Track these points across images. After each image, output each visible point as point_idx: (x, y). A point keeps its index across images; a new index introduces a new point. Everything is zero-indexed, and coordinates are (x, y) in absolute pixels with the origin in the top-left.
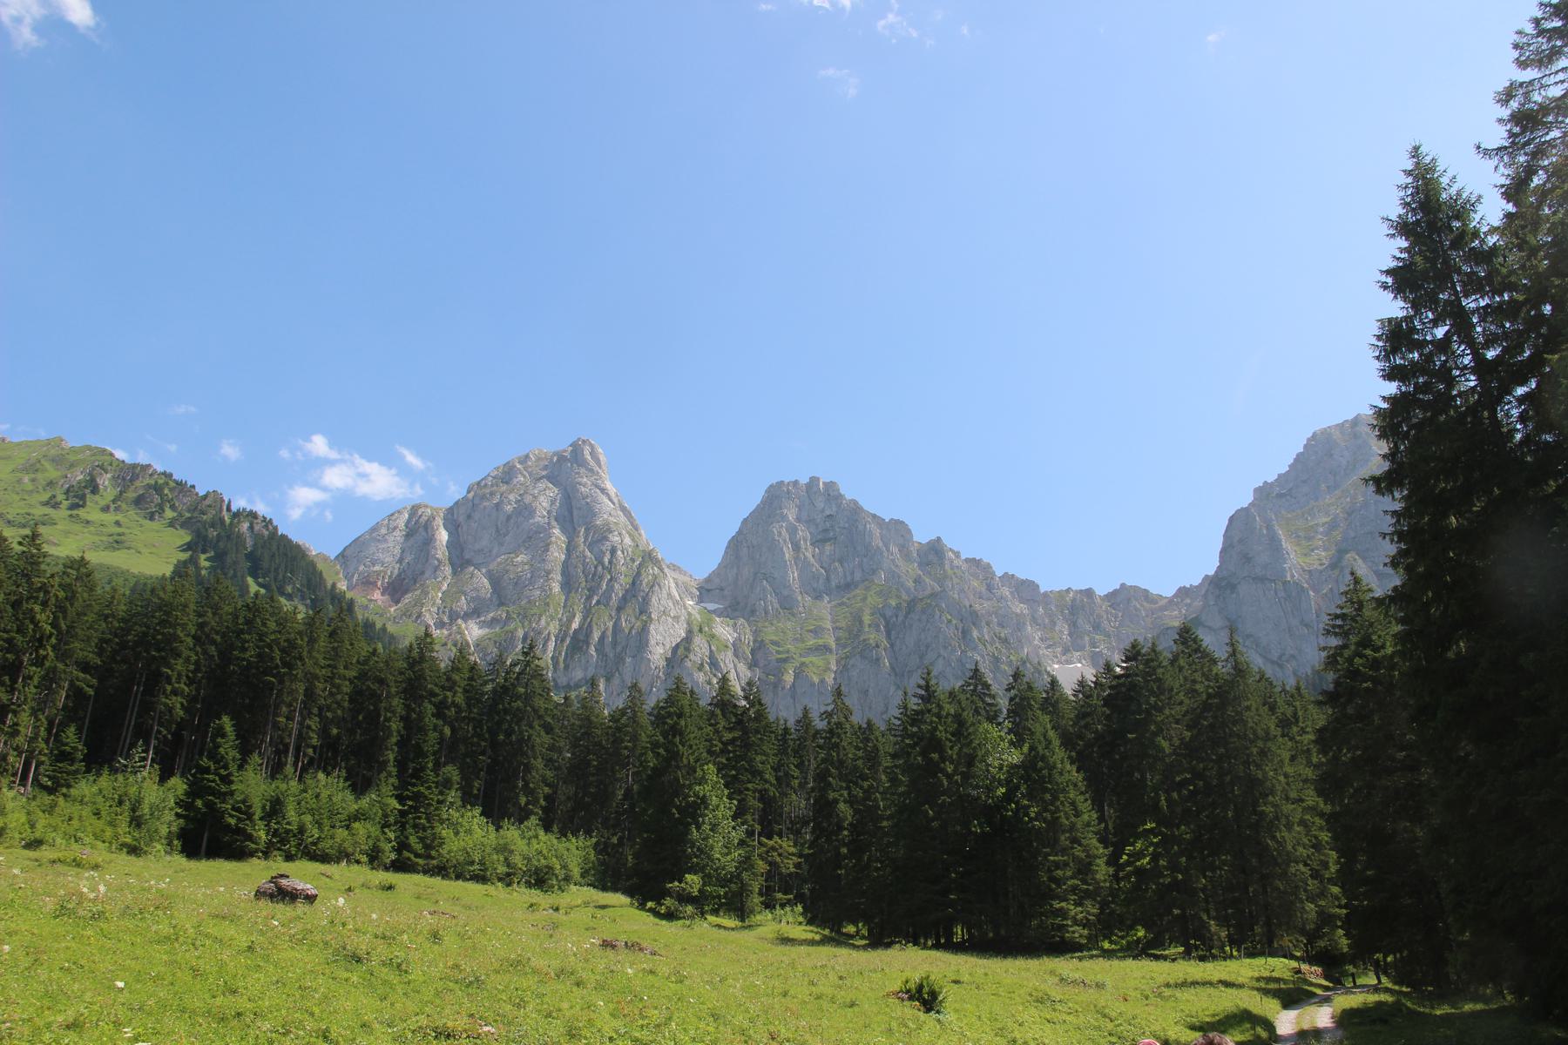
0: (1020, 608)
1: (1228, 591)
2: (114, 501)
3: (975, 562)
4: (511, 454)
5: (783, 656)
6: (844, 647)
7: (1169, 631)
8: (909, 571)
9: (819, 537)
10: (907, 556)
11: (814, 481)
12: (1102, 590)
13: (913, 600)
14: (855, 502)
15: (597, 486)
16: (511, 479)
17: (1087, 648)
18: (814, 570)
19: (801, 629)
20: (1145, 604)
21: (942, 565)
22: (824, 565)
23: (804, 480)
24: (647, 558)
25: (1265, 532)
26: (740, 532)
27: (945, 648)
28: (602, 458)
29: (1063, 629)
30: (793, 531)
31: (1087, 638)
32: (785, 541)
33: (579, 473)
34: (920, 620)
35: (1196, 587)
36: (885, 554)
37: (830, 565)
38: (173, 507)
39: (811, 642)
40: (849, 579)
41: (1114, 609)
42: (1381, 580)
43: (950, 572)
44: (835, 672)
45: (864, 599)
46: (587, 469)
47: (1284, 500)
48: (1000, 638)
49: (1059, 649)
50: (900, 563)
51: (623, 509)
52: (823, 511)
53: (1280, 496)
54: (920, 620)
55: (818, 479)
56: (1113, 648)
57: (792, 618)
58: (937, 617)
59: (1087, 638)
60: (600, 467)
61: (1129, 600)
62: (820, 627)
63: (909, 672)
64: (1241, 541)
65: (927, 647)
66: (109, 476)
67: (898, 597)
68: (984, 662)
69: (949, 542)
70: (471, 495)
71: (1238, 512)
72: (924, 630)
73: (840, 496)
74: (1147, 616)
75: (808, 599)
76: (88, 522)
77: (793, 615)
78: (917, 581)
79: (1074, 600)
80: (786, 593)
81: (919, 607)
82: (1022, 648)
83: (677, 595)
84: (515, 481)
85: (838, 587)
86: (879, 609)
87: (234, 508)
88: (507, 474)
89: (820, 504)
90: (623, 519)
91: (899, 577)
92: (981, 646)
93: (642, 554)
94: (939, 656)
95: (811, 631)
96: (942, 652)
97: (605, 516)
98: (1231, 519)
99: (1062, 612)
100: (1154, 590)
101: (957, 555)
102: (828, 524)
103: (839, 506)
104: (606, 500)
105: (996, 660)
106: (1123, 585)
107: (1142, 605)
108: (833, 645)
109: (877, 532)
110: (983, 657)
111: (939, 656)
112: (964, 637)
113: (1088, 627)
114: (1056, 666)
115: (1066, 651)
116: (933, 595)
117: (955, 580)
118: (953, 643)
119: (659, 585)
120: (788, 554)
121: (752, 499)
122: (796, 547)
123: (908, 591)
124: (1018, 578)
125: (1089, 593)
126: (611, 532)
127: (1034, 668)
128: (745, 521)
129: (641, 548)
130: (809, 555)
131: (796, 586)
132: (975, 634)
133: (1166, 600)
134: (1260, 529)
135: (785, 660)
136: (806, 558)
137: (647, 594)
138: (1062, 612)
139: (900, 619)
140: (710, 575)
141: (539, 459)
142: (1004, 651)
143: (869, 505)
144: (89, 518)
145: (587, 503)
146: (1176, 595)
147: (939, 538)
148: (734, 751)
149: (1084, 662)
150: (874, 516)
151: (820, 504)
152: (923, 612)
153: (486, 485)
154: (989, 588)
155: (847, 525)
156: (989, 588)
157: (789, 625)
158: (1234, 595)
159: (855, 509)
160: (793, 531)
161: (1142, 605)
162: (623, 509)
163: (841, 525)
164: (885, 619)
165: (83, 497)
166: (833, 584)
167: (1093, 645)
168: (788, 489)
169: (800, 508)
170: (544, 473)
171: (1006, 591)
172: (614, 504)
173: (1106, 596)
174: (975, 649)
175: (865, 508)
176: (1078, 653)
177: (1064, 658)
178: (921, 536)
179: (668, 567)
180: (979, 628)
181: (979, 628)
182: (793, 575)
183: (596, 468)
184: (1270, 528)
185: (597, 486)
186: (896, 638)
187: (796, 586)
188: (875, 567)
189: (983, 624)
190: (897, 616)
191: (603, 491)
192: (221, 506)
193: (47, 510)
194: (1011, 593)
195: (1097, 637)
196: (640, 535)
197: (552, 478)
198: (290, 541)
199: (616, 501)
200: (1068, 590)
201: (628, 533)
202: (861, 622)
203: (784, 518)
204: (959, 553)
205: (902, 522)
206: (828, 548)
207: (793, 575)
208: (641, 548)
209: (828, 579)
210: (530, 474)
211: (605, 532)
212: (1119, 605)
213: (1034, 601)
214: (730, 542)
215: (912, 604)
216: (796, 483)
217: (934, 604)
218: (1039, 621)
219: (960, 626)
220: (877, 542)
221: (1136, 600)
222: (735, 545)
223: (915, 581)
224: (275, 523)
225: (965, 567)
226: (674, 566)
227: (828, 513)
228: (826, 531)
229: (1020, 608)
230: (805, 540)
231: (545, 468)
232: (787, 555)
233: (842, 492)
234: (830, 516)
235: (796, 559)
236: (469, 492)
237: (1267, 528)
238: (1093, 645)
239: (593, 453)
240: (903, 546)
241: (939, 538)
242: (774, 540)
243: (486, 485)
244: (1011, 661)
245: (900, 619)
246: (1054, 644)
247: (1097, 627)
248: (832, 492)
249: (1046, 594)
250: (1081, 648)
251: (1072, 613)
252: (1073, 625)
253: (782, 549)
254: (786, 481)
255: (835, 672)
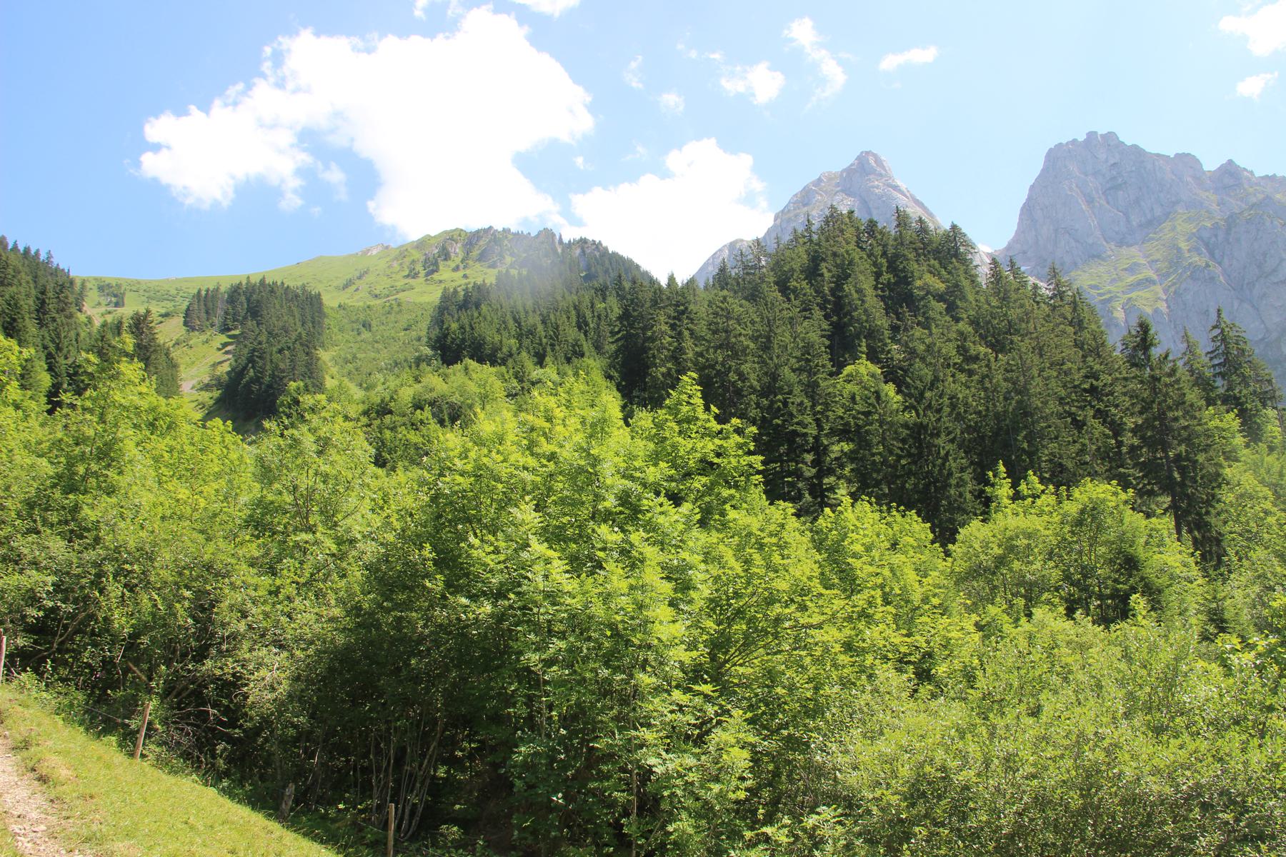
2: (462, 261)
5: (1107, 297)
6: (1168, 275)
11: (1091, 135)
13: (1231, 216)
19: (1115, 269)
26: (1029, 199)
38: (512, 255)
39: (1131, 279)
40: (1149, 216)
44: (1166, 300)
45: (1173, 229)
52: (1107, 161)
58: (1268, 224)
62: (1135, 264)
63: (1248, 284)
65: (1265, 255)
66: (459, 245)
69: (1241, 162)
70: (779, 221)
76: (441, 282)
77: (1104, 260)
84: (814, 201)
85: (1140, 226)
86: (1193, 234)
87: (566, 240)
95: (1126, 269)
104: (900, 196)
108: (1155, 277)
128: (1032, 188)
135: (1109, 300)
139: (1220, 238)
140: (1009, 243)
143: (1151, 147)
144: (441, 278)
148: (873, 455)
153: (789, 211)
157: (1102, 269)
164: (1203, 241)
165: (436, 264)
166: (1134, 223)
178: (1211, 163)
185: (889, 186)
190: (1216, 236)
192: (553, 241)
193: (407, 281)
198: (622, 258)
202: (1179, 250)
214: (1022, 209)
222: (1028, 211)
224: (604, 245)
228: (1114, 178)
231: (838, 185)
236: (775, 220)
243: (789, 211)
245: (1220, 238)
255: (1166, 300)
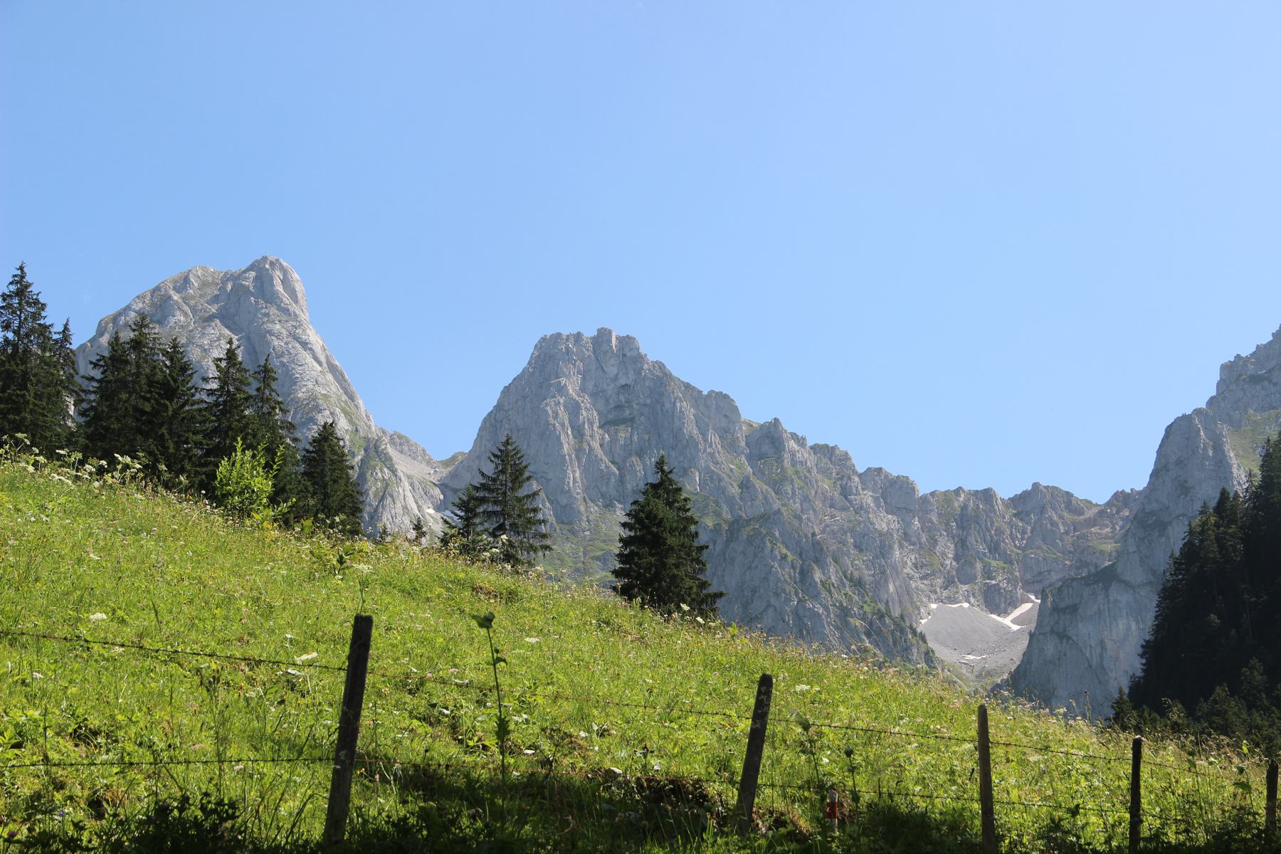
0: (885, 522)
1: (1156, 534)
3: (824, 451)
4: (161, 273)
7: (1074, 584)
8: (734, 467)
9: (611, 417)
10: (731, 446)
11: (604, 334)
12: (1006, 490)
14: (661, 366)
15: (297, 339)
16: (165, 318)
17: (979, 580)
18: (603, 467)
19: (585, 554)
20: (1065, 514)
21: (780, 459)
22: (617, 459)
23: (589, 332)
24: (372, 453)
25: (1211, 453)
26: (499, 407)
27: (777, 595)
28: (299, 287)
29: (947, 548)
30: (574, 409)
31: (979, 566)
32: (563, 425)
33: (267, 315)
34: (744, 553)
35: (1139, 493)
36: (701, 447)
37: (624, 462)
41: (1022, 520)
42: (1139, 674)
43: (790, 471)
46: (279, 308)
47: (1258, 387)
48: (851, 580)
49: (939, 581)
50: (721, 458)
51: (333, 369)
52: (616, 378)
53: (1255, 379)
54: (744, 553)
55: (610, 332)
56: (1016, 580)
57: (572, 537)
58: (767, 551)
59: (979, 566)
60: (296, 302)
61: (1043, 510)
64: (1179, 462)
65: (754, 591)
67: (718, 514)
68: (828, 616)
71: (1178, 420)
72: (749, 568)
73: (640, 358)
74: (1067, 533)
75: (594, 508)
77: (573, 532)
78: (745, 485)
79: (964, 508)
80: (564, 501)
81: (744, 535)
82: (886, 581)
83: (414, 506)
84: (172, 320)
88: (161, 304)
89: (612, 370)
90: (334, 388)
91: (720, 480)
92: (824, 594)
93: (364, 444)
94: (769, 605)
95: (597, 558)
96: (773, 601)
97: (310, 385)
98: (1169, 429)
99: (947, 524)
100: (1080, 493)
101: (801, 441)
102: (622, 398)
103: (638, 372)
104: (310, 360)
105: (844, 613)
106: (1036, 485)
107: (1061, 517)
109: (689, 411)
110: (826, 608)
111: (769, 605)
112: (802, 581)
113: (982, 548)
114: (934, 606)
115: (949, 583)
116: (765, 518)
117: (798, 483)
118: (787, 588)
119: (392, 496)
120: (567, 443)
121: (515, 362)
122: (579, 433)
123: (730, 502)
124: (887, 475)
125: (987, 495)
126: (320, 411)
127: (895, 624)
128: (507, 390)
129: (362, 434)
130: (596, 445)
131: (578, 491)
132: (818, 576)
133: (1095, 510)
134: (1205, 449)
136: (591, 449)
137: (376, 510)
138: (947, 524)
141: (204, 284)
142: (856, 598)
143: (682, 370)
145: (283, 364)
146: (1109, 504)
147: (776, 420)
149: (972, 600)
150: (687, 386)
151: (612, 370)
152: (750, 541)
154: (845, 492)
155: (648, 401)
156: (845, 492)
158: (1163, 539)
159: (662, 379)
160: (574, 409)
161: (1061, 517)
162: (333, 369)
163: (641, 401)
166: (629, 486)
167: (988, 574)
168: (567, 348)
169: (585, 375)
170: (213, 309)
171: (867, 498)
172: (320, 364)
173: (1011, 499)
174: (816, 597)
175: (675, 374)
176: (965, 587)
177: (945, 593)
179: (392, 441)
180: (823, 567)
181: (823, 567)
182: (574, 476)
183: (293, 308)
184: (1218, 448)
185: (297, 339)
186: (714, 574)
187: (578, 491)
188: (686, 465)
189: (829, 560)
191: (305, 345)
194: (876, 499)
195: (994, 563)
196: (357, 407)
197: (227, 318)
199: (323, 359)
200: (958, 491)
201: (344, 411)
203: (561, 390)
204: (804, 439)
205: (726, 396)
206: (623, 434)
207: (574, 476)
208: (362, 434)
209: (622, 480)
210: (194, 310)
211: (312, 410)
212: (1028, 514)
213: (910, 511)
214: (485, 420)
215: (736, 525)
216: (578, 337)
217: (763, 531)
218: (914, 539)
219: (798, 563)
220: (691, 429)
221: (1054, 509)
223: (741, 486)
225: (811, 460)
226: (400, 437)
227: (623, 381)
229: (885, 522)
230: (591, 424)
231: (215, 299)
232: (566, 447)
233: (642, 351)
234: (625, 386)
235: (579, 451)
237: (1214, 448)
238: (988, 574)
239: (286, 282)
240: (726, 431)
241: (776, 420)
242: (548, 424)
244: (865, 613)
246: (933, 574)
247: (995, 548)
248: (628, 352)
249: (924, 499)
250: (969, 579)
251: (961, 527)
252: (962, 544)
253: (558, 438)
254: (565, 333)
